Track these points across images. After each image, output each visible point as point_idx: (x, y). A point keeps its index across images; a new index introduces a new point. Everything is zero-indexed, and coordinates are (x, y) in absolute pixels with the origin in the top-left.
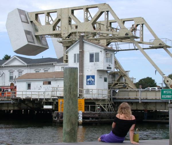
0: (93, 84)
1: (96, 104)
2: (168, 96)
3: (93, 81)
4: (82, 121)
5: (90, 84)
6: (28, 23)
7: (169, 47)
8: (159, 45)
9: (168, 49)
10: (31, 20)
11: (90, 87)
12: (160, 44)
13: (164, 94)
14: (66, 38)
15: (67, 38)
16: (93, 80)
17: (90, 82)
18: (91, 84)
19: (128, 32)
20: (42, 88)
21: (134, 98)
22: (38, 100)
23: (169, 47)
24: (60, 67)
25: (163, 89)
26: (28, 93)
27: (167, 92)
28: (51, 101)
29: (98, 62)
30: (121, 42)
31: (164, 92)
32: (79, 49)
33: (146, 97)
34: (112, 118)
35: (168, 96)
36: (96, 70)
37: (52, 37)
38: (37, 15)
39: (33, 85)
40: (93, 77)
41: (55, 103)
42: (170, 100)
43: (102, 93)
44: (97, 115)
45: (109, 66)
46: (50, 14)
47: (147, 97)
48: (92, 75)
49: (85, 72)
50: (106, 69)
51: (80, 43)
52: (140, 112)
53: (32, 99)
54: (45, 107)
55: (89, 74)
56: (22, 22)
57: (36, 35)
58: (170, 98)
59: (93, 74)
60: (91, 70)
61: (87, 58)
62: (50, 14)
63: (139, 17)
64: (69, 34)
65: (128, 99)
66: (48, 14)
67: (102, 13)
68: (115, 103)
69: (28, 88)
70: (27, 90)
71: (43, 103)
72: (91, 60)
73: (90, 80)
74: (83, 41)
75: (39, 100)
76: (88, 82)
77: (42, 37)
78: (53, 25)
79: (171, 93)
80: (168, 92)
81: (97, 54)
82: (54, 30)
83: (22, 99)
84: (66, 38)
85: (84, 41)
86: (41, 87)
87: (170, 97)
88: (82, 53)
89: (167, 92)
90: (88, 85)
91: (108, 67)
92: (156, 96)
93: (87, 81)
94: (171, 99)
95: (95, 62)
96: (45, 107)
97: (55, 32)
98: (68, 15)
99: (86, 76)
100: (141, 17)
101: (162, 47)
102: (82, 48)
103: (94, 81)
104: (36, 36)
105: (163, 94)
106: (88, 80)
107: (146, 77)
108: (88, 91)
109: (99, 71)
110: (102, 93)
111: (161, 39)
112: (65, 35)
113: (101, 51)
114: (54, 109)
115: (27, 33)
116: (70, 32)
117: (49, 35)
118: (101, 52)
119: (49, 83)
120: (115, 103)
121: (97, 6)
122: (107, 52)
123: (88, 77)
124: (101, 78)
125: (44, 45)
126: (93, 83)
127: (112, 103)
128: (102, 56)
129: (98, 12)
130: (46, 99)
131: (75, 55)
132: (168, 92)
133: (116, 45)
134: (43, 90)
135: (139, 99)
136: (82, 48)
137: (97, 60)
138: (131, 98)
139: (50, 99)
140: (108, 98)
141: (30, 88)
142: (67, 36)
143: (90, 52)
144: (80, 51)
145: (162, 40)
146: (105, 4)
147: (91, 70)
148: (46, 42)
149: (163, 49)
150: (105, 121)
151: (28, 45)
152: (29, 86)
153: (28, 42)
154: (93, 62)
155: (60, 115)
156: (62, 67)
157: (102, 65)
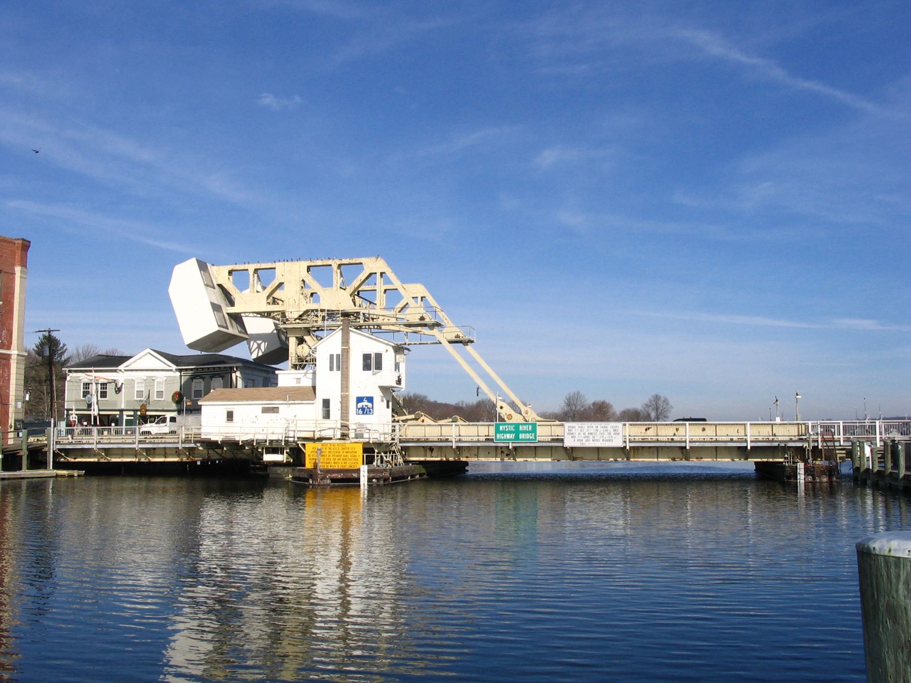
2: (508, 436)
3: (369, 408)
5: (363, 414)
6: (214, 288)
8: (456, 337)
11: (364, 419)
13: (501, 432)
15: (298, 321)
16: (370, 405)
17: (363, 409)
18: (366, 413)
27: (506, 428)
31: (501, 428)
35: (508, 436)
37: (256, 317)
40: (370, 399)
53: (242, 442)
54: (268, 458)
61: (356, 362)
72: (367, 367)
81: (379, 356)
83: (219, 443)
86: (256, 417)
87: (511, 437)
88: (346, 352)
89: (506, 428)
93: (357, 408)
96: (268, 458)
102: (346, 341)
103: (373, 408)
106: (360, 405)
107: (444, 403)
109: (385, 390)
115: (216, 308)
123: (360, 400)
126: (370, 411)
128: (389, 358)
130: (271, 441)
131: (332, 356)
135: (452, 442)
136: (346, 341)
137: (379, 366)
140: (401, 441)
141: (232, 420)
142: (296, 316)
144: (342, 349)
150: (649, 462)
151: (219, 332)
153: (219, 326)
155: (320, 476)
157: (387, 376)
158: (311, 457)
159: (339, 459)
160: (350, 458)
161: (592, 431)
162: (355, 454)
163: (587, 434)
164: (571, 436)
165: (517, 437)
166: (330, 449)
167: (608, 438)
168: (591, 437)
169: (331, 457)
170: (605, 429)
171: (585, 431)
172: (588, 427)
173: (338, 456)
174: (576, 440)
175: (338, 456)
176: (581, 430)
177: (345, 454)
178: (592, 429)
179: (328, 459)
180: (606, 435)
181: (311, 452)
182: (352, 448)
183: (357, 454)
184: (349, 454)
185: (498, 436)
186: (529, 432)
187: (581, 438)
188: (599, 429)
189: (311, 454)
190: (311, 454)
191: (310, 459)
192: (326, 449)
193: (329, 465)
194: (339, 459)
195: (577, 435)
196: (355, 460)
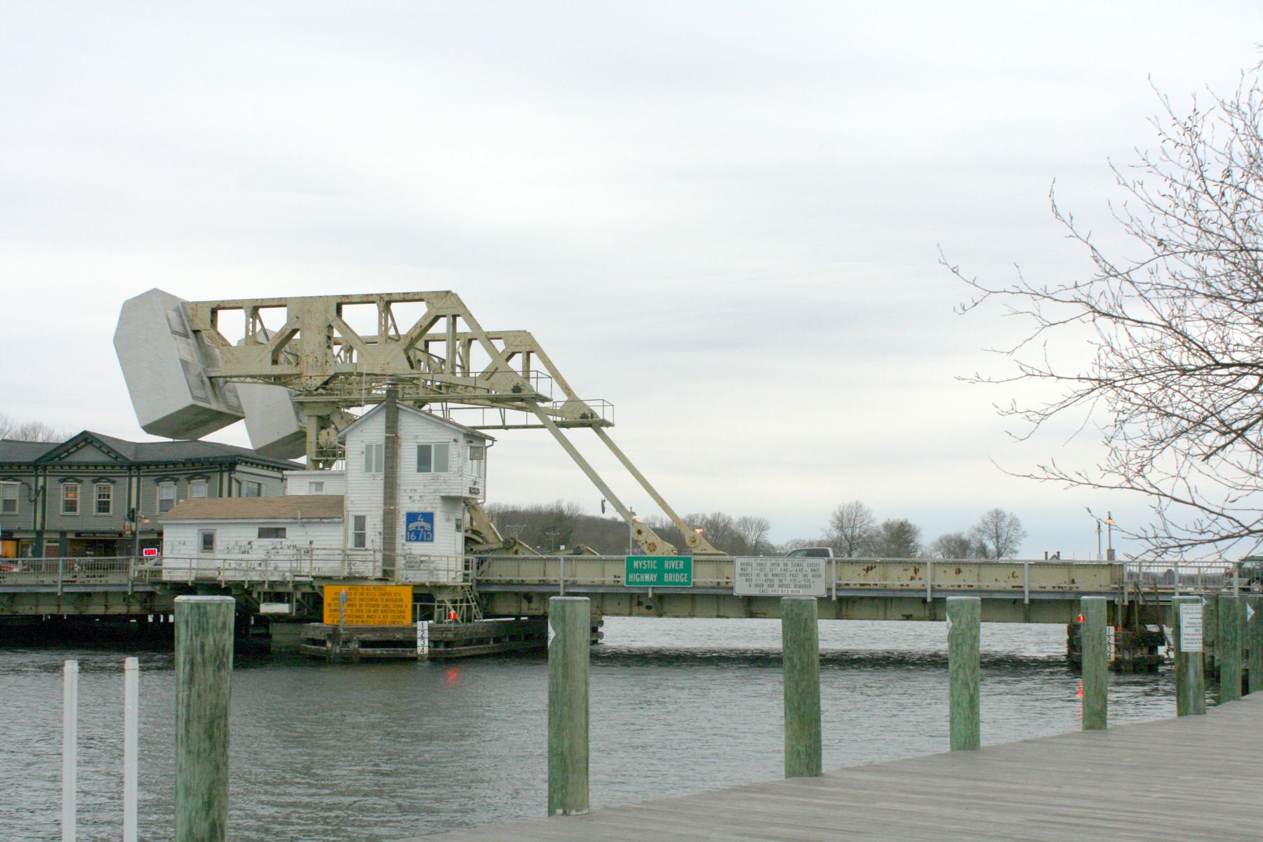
0: (427, 541)
1: (434, 599)
2: (647, 577)
3: (426, 531)
4: (426, 650)
5: (417, 540)
7: (609, 425)
9: (604, 429)
10: (196, 328)
11: (418, 548)
12: (584, 416)
14: (316, 390)
15: (321, 391)
16: (427, 525)
17: (417, 533)
18: (422, 540)
19: (521, 383)
20: (254, 547)
21: (537, 582)
22: (243, 586)
23: (609, 425)
24: (306, 482)
25: (631, 555)
26: (204, 564)
27: (643, 565)
28: (290, 588)
29: (443, 474)
30: (462, 403)
31: (636, 564)
32: (384, 430)
33: (572, 579)
34: (474, 641)
35: (647, 577)
36: (438, 497)
38: (214, 312)
39: (223, 538)
40: (429, 517)
41: (299, 596)
42: (653, 588)
43: (448, 564)
44: (450, 636)
45: (475, 483)
46: (261, 311)
47: (575, 579)
48: (422, 510)
49: (1201, 611)
50: (468, 495)
51: (387, 413)
52: (513, 619)
55: (416, 508)
56: (174, 332)
57: (213, 374)
58: (651, 583)
59: (429, 510)
60: (421, 497)
62: (261, 311)
63: (519, 331)
64: (327, 378)
65: (540, 585)
66: (254, 310)
67: (437, 318)
68: (481, 594)
69: (205, 549)
70: (203, 555)
71: (255, 595)
73: (417, 527)
74: (398, 405)
75: (246, 587)
76: (411, 532)
77: (226, 382)
78: (274, 347)
79: (655, 568)
80: (647, 563)
81: (443, 449)
82: (275, 362)
84: (316, 390)
85: (398, 408)
86: (249, 543)
87: (652, 578)
88: (392, 442)
89: (643, 565)
90: (410, 540)
91: (472, 486)
92: (603, 576)
93: (407, 530)
94: (654, 583)
95: (435, 471)
96: (266, 608)
97: (277, 370)
98: (327, 319)
99: (404, 513)
100: (524, 329)
101: (590, 425)
104: (210, 378)
105: (630, 569)
106: (413, 526)
108: (412, 564)
109: (450, 501)
110: (448, 564)
111: (586, 402)
112: (315, 382)
113: (455, 440)
114: (294, 614)
116: (331, 373)
117: (252, 377)
118: (454, 443)
119: (278, 533)
120: (481, 594)
121: (422, 297)
122: (471, 442)
123: (412, 517)
124: (448, 520)
125: (229, 407)
126: (428, 536)
127: (475, 596)
129: (425, 317)
131: (369, 447)
132: (647, 563)
133: (443, 410)
134: (257, 554)
137: (443, 466)
138: (526, 582)
139: (283, 583)
141: (211, 549)
143: (418, 441)
145: (588, 403)
146: (449, 294)
147: (421, 497)
148: (237, 397)
149: (590, 428)
151: (193, 406)
152: (208, 542)
153: (195, 397)
154: (430, 471)
155: (343, 637)
156: (312, 481)
158: (333, 608)
159: (376, 611)
160: (392, 608)
161: (778, 571)
162: (401, 603)
163: (770, 576)
164: (744, 578)
165: (660, 579)
166: (362, 594)
167: (803, 583)
168: (776, 579)
169: (364, 608)
170: (798, 568)
171: (768, 570)
172: (773, 564)
173: (373, 606)
174: (753, 583)
175: (373, 606)
176: (761, 570)
177: (385, 603)
178: (779, 568)
179: (357, 611)
180: (800, 578)
181: (333, 600)
182: (395, 594)
183: (404, 604)
184: (391, 603)
185: (631, 577)
186: (679, 571)
187: (759, 582)
188: (789, 567)
189: (333, 603)
190: (333, 603)
191: (331, 610)
192: (356, 594)
193: (360, 620)
194: (376, 611)
195: (754, 577)
196: (401, 612)
